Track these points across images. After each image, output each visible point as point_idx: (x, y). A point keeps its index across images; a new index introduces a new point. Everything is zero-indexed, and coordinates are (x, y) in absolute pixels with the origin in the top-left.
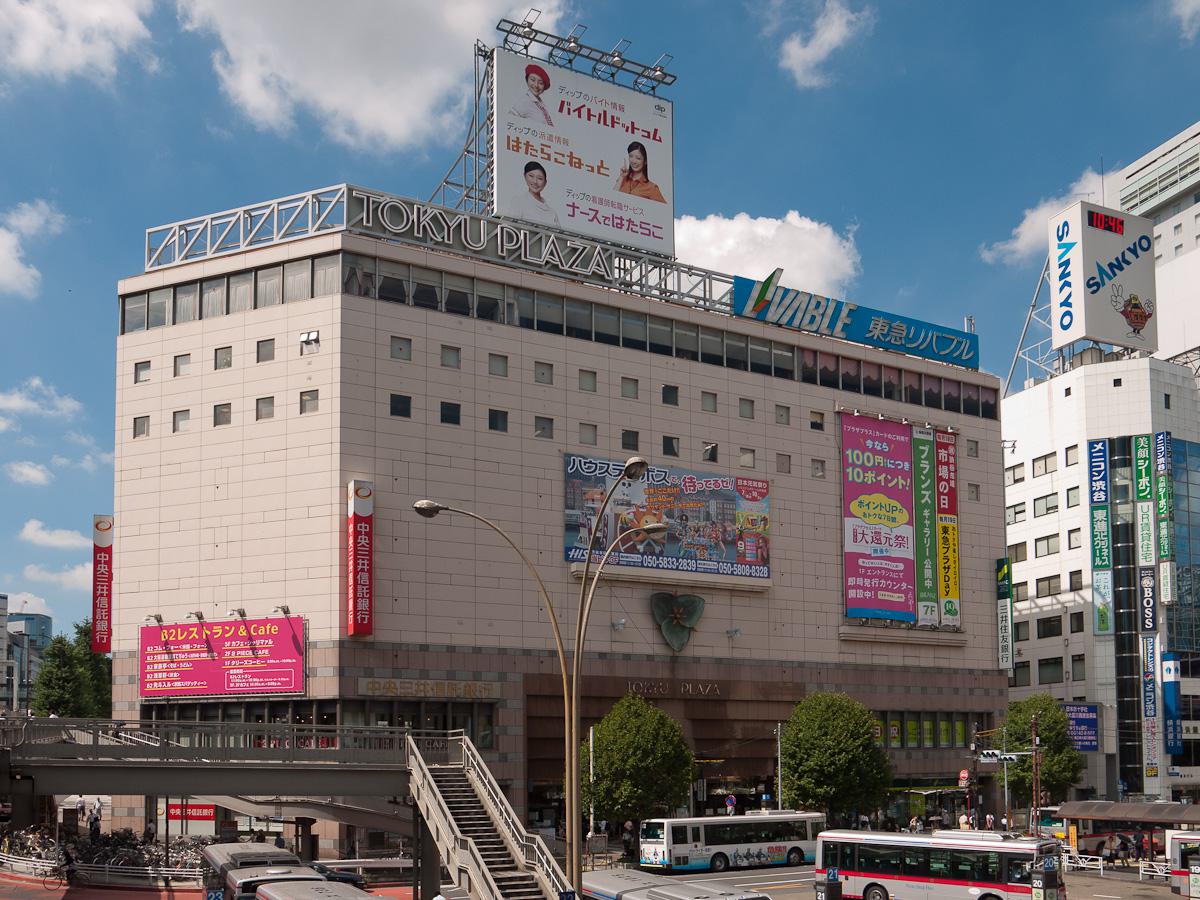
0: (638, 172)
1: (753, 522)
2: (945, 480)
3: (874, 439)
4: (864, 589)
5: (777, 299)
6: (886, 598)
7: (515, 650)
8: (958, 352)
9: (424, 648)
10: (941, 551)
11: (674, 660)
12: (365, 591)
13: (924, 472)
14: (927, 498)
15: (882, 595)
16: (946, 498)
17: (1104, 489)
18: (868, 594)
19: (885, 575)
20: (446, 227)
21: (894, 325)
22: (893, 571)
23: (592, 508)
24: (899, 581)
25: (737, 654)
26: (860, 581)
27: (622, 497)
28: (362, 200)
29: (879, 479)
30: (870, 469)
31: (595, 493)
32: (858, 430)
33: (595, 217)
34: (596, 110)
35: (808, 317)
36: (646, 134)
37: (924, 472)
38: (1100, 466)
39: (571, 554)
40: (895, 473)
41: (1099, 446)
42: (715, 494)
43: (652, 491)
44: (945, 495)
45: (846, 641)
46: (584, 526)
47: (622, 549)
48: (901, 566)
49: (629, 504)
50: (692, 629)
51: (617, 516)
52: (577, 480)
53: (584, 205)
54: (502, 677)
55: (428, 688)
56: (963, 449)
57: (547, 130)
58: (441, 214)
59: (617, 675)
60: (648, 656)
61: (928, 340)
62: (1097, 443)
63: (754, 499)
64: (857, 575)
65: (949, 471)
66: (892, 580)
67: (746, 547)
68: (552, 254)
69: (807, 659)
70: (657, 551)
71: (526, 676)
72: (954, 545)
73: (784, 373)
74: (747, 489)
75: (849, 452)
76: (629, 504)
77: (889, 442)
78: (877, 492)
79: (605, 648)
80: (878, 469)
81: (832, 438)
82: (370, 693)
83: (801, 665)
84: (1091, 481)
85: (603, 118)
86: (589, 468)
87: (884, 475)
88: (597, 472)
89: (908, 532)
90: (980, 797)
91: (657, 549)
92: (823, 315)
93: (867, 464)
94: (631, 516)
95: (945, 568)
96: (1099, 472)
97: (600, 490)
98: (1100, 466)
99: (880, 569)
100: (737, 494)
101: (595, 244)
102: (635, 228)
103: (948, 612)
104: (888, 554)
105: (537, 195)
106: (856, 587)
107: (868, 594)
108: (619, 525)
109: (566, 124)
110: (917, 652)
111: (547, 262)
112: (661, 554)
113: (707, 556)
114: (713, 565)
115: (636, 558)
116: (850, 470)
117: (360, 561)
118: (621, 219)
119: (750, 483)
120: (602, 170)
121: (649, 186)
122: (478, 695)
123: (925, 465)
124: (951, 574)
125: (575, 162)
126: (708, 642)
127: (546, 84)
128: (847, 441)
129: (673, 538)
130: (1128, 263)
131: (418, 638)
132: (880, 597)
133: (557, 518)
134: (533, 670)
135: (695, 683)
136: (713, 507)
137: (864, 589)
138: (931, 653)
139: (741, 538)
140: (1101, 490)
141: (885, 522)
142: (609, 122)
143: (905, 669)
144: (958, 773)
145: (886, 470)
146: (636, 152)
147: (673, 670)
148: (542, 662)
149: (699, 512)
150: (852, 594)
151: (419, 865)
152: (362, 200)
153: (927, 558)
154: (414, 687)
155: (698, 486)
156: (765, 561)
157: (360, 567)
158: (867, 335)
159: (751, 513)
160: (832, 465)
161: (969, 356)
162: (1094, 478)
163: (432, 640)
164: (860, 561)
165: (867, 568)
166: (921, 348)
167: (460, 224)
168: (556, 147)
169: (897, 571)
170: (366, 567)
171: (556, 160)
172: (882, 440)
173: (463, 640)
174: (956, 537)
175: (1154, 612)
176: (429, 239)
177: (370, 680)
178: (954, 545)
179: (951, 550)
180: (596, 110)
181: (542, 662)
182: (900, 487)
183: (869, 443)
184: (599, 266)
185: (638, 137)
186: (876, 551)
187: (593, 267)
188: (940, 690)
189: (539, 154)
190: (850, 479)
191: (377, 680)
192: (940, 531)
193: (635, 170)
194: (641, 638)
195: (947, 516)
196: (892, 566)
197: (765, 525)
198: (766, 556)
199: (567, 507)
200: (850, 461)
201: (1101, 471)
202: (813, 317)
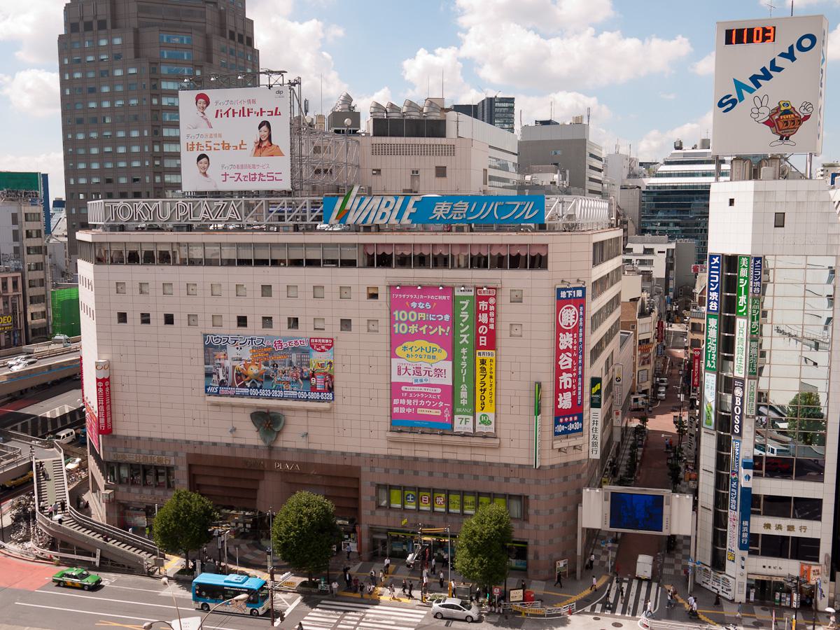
0: (265, 141)
1: (322, 366)
2: (485, 324)
3: (417, 301)
4: (406, 406)
5: (355, 207)
6: (425, 413)
7: (181, 440)
8: (521, 214)
9: (138, 438)
10: (479, 378)
11: (271, 448)
13: (464, 321)
14: (465, 340)
15: (420, 411)
16: (485, 337)
17: (717, 300)
18: (409, 410)
19: (426, 397)
21: (456, 205)
22: (432, 394)
23: (220, 364)
24: (438, 401)
25: (312, 447)
26: (403, 402)
27: (236, 356)
29: (421, 329)
30: (414, 323)
31: (221, 354)
32: (404, 296)
33: (239, 177)
34: (238, 108)
35: (380, 214)
36: (270, 113)
37: (464, 321)
39: (208, 390)
40: (435, 324)
42: (295, 349)
43: (254, 351)
44: (484, 335)
45: (391, 441)
46: (215, 374)
47: (237, 386)
48: (439, 390)
49: (241, 360)
50: (279, 432)
51: (234, 367)
52: (212, 348)
53: (231, 172)
54: (176, 454)
55: (141, 458)
56: (504, 299)
57: (210, 131)
59: (237, 456)
60: (255, 446)
61: (490, 209)
62: (715, 257)
63: (322, 351)
64: (400, 398)
65: (489, 317)
66: (431, 400)
67: (318, 382)
68: (205, 213)
69: (362, 451)
70: (258, 386)
71: (188, 455)
72: (491, 373)
73: (350, 263)
74: (316, 345)
75: (396, 313)
76: (241, 360)
77: (431, 302)
78: (420, 339)
79: (229, 441)
80: (420, 323)
81: (385, 304)
83: (358, 455)
85: (242, 113)
86: (217, 341)
87: (426, 326)
88: (222, 343)
89: (448, 366)
90: (442, 574)
91: (259, 385)
92: (392, 211)
93: (406, 326)
94: (242, 366)
95: (481, 390)
97: (224, 353)
99: (420, 393)
100: (311, 348)
102: (263, 178)
103: (482, 422)
104: (428, 382)
105: (205, 174)
106: (399, 405)
107: (409, 410)
108: (235, 372)
109: (221, 124)
110: (455, 450)
111: (204, 218)
112: (261, 387)
113: (290, 388)
114: (294, 394)
115: (245, 391)
116: (396, 326)
118: (255, 174)
119: (320, 340)
120: (243, 147)
121: (273, 147)
123: (465, 315)
124: (487, 394)
125: (226, 146)
126: (291, 439)
127: (208, 103)
128: (395, 305)
129: (268, 378)
130: (779, 69)
131: (134, 434)
132: (418, 412)
133: (201, 370)
134: (191, 451)
135: (284, 463)
136: (294, 357)
137: (406, 406)
138: (468, 451)
139: (313, 375)
141: (426, 360)
142: (246, 113)
143: (445, 461)
144: (335, 581)
145: (428, 322)
146: (264, 128)
147: (270, 454)
149: (285, 361)
150: (396, 410)
153: (463, 383)
155: (284, 346)
156: (331, 389)
158: (431, 218)
159: (321, 360)
160: (384, 323)
161: (531, 216)
162: (712, 289)
163: (142, 434)
164: (403, 388)
165: (409, 393)
166: (482, 218)
167: (156, 208)
168: (214, 140)
169: (436, 394)
171: (215, 149)
172: (424, 301)
174: (493, 367)
175: (741, 420)
178: (491, 373)
179: (488, 377)
180: (238, 108)
182: (440, 334)
183: (414, 305)
185: (265, 117)
186: (416, 381)
188: (476, 477)
189: (205, 148)
190: (396, 332)
192: (478, 362)
193: (263, 139)
194: (250, 436)
195: (488, 351)
196: (431, 390)
197: (331, 367)
198: (330, 386)
199: (206, 364)
200: (397, 319)
201: (717, 283)
202: (384, 214)
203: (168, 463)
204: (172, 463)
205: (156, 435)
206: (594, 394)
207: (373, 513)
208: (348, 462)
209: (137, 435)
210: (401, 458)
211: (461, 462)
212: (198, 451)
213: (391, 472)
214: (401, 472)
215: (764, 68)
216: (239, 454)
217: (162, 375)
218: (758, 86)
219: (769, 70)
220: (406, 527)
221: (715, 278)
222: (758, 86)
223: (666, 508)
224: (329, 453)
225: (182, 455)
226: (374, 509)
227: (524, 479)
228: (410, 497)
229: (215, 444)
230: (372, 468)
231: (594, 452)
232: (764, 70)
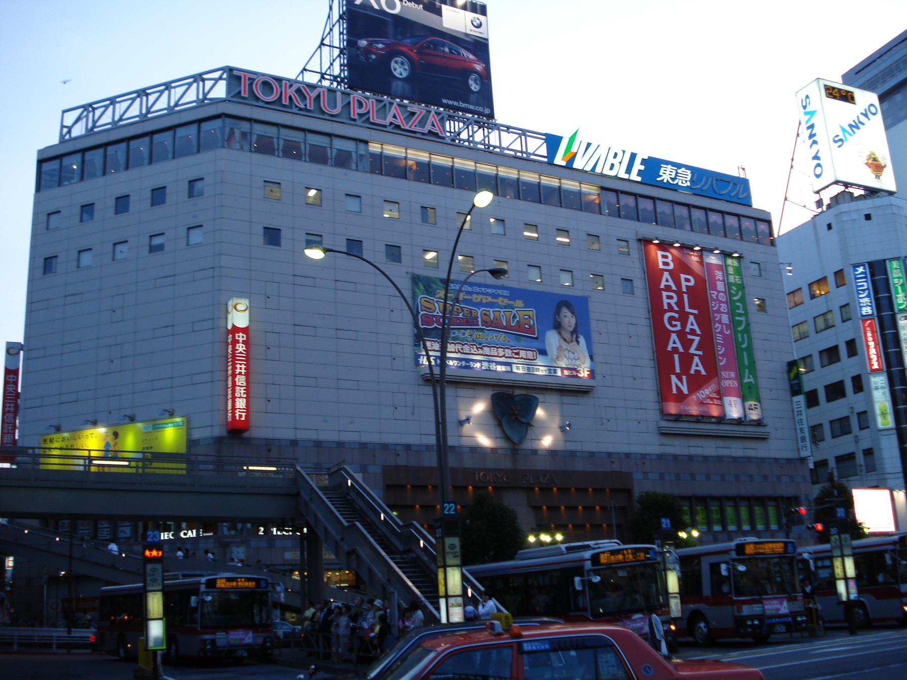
7: (374, 444)
21: (679, 171)
83: (628, 455)
117: (238, 366)
130: (863, 124)
131: (289, 435)
187: (428, 127)
205: (328, 435)
208: (616, 467)
209: (292, 437)
210: (675, 457)
211: (735, 459)
212: (401, 461)
218: (808, 128)
221: (863, 286)
224: (592, 454)
225: (375, 469)
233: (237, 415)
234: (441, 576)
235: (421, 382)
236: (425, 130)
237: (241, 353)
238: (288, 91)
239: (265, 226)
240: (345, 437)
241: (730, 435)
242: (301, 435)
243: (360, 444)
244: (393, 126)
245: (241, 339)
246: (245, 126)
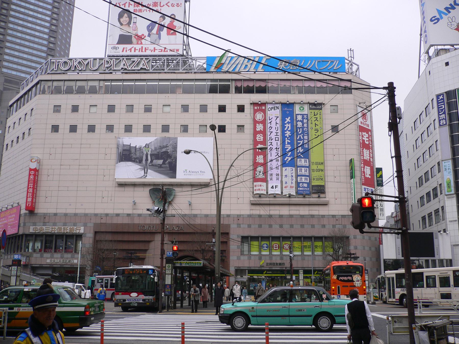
5: (227, 62)
7: (91, 214)
9: (55, 214)
12: (31, 195)
17: (445, 118)
20: (83, 64)
25: (194, 212)
28: (54, 62)
35: (244, 66)
36: (160, 51)
38: (442, 107)
41: (441, 97)
58: (81, 60)
68: (124, 65)
69: (232, 213)
79: (130, 212)
82: (34, 232)
84: (439, 115)
96: (442, 110)
98: (442, 107)
101: (124, 57)
117: (30, 185)
122: (75, 232)
131: (54, 211)
134: (98, 221)
138: (307, 208)
140: (443, 119)
143: (291, 216)
148: (102, 218)
151: (152, 280)
152: (54, 62)
154: (51, 229)
157: (30, 186)
162: (440, 113)
167: (89, 62)
170: (32, 186)
173: (71, 211)
176: (77, 70)
177: (34, 227)
181: (102, 218)
184: (144, 65)
187: (141, 66)
188: (313, 226)
191: (37, 227)
201: (443, 109)
203: (78, 231)
204: (82, 231)
206: (379, 178)
207: (239, 258)
209: (55, 212)
211: (302, 216)
212: (103, 221)
213: (252, 226)
214: (260, 226)
215: (451, 4)
216: (137, 221)
217: (81, 167)
218: (449, 12)
219: (453, 5)
220: (263, 267)
222: (449, 12)
223: (435, 240)
225: (91, 225)
226: (240, 255)
227: (346, 225)
228: (265, 246)
229: (118, 215)
230: (239, 225)
231: (382, 215)
232: (451, 5)
233: (28, 204)
234: (295, 269)
235: (117, 185)
236: (139, 68)
237: (32, 179)
238: (74, 64)
239: (238, 125)
240: (78, 211)
241: (282, 203)
242: (59, 211)
243: (95, 214)
244: (123, 69)
245: (32, 173)
246: (50, 84)
